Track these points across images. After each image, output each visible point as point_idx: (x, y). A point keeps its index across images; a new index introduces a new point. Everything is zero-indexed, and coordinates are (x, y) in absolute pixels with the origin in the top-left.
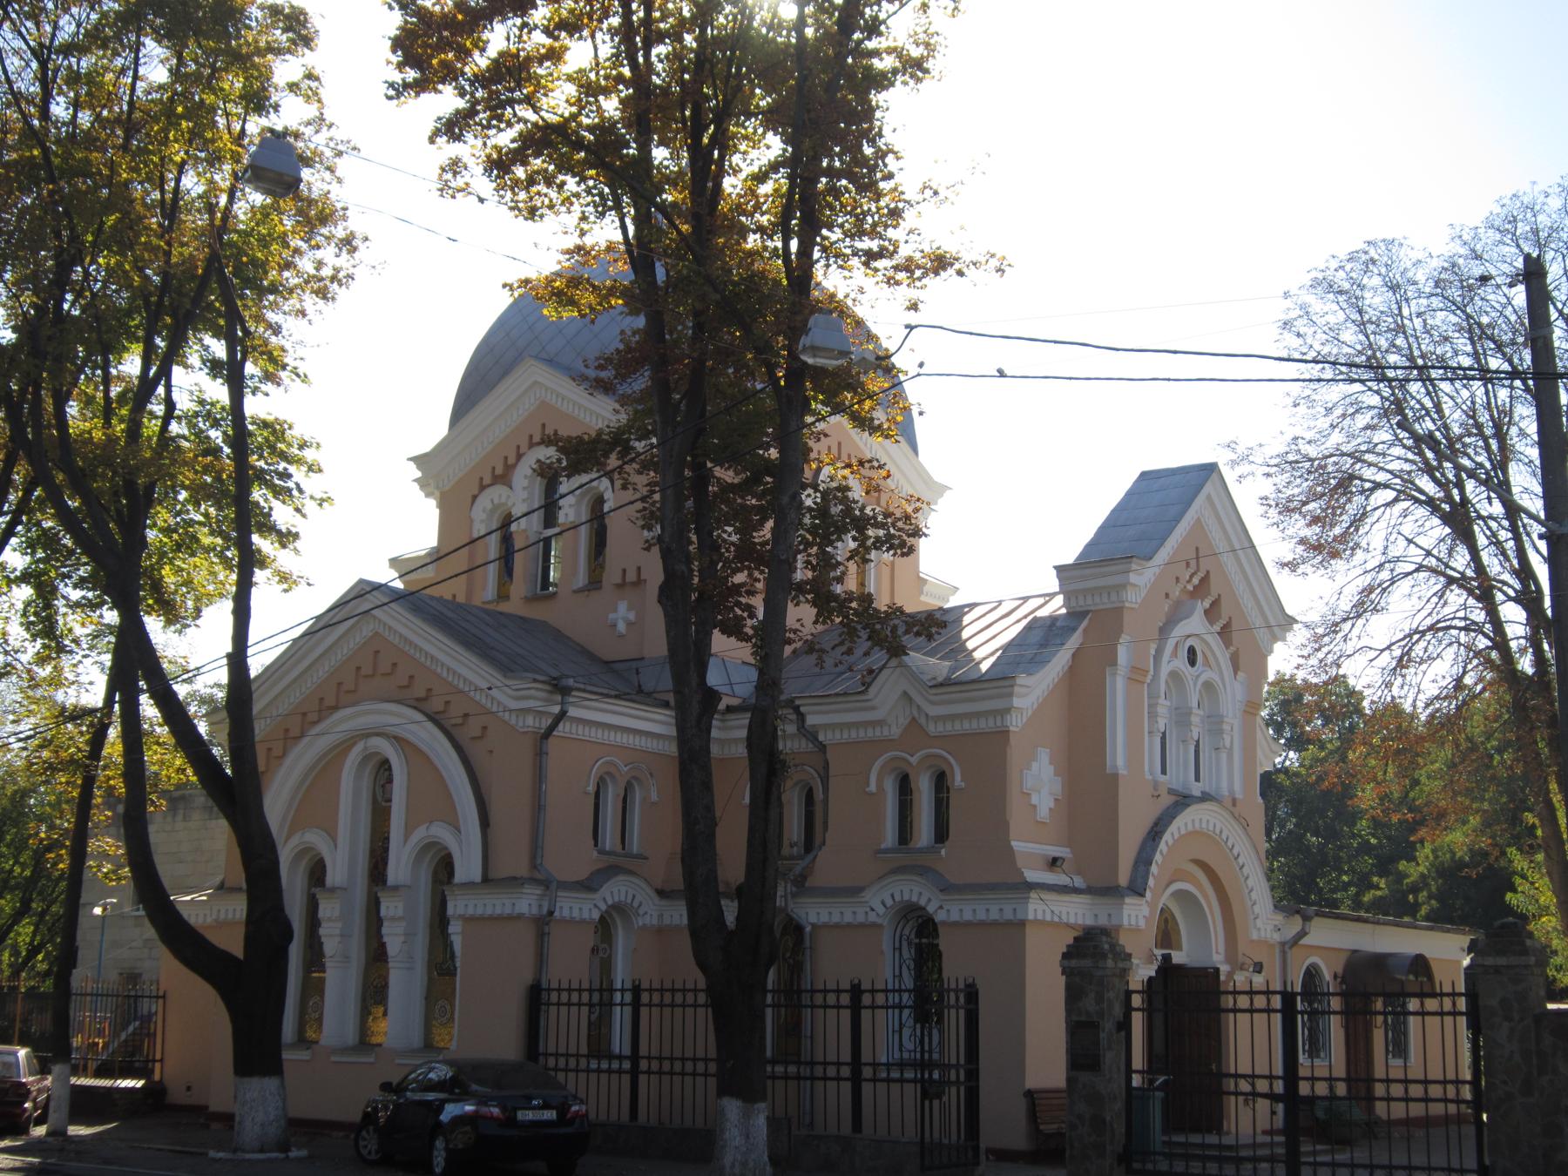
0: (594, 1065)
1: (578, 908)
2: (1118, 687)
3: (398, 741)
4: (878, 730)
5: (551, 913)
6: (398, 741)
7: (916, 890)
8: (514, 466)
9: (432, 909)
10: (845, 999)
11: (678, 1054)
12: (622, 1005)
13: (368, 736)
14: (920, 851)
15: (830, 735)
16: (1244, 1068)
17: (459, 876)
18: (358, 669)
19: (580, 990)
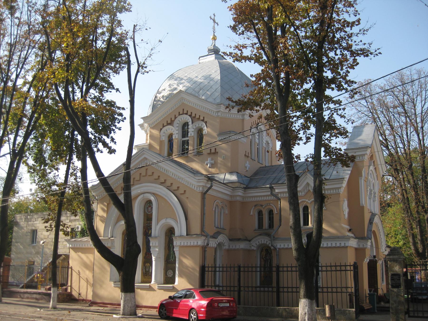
0: (221, 288)
1: (213, 243)
2: (362, 183)
3: (154, 194)
4: (260, 198)
5: (208, 245)
6: (154, 194)
7: (266, 241)
8: (174, 121)
9: (165, 244)
10: (236, 269)
11: (250, 285)
12: (219, 271)
13: (144, 193)
14: (266, 230)
15: (329, 192)
16: (286, 285)
17: (177, 233)
18: (140, 174)
19: (212, 267)
